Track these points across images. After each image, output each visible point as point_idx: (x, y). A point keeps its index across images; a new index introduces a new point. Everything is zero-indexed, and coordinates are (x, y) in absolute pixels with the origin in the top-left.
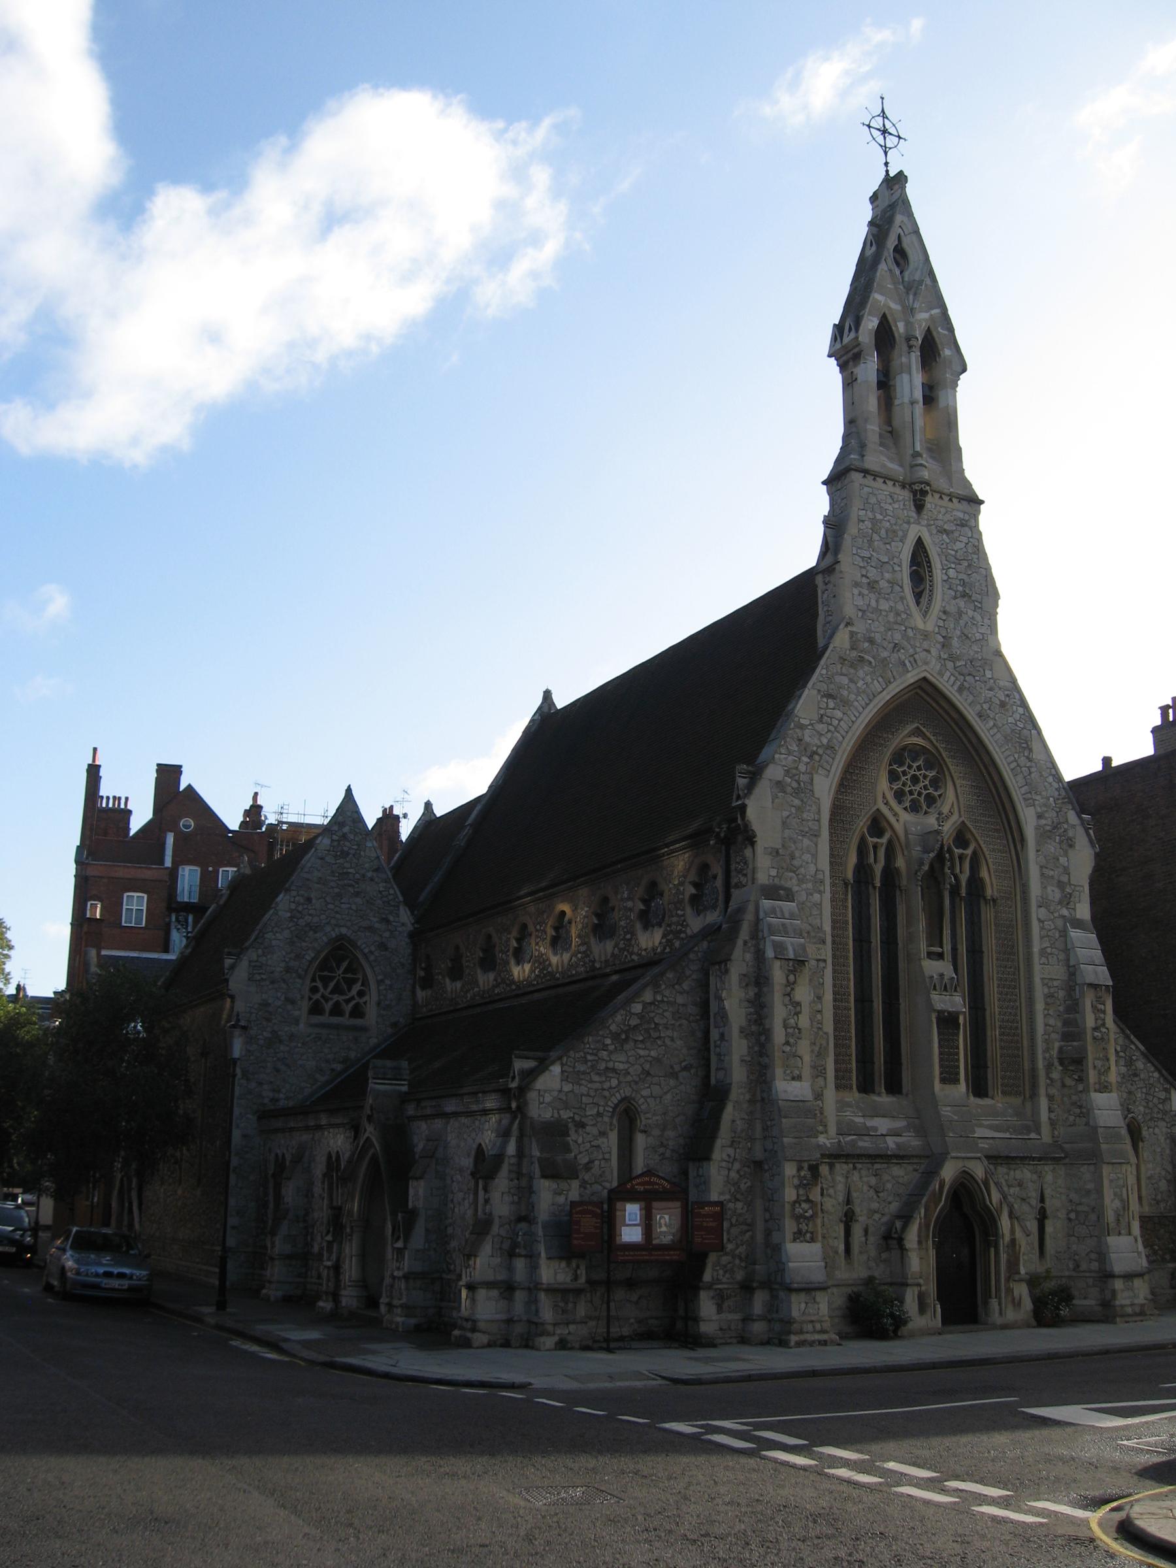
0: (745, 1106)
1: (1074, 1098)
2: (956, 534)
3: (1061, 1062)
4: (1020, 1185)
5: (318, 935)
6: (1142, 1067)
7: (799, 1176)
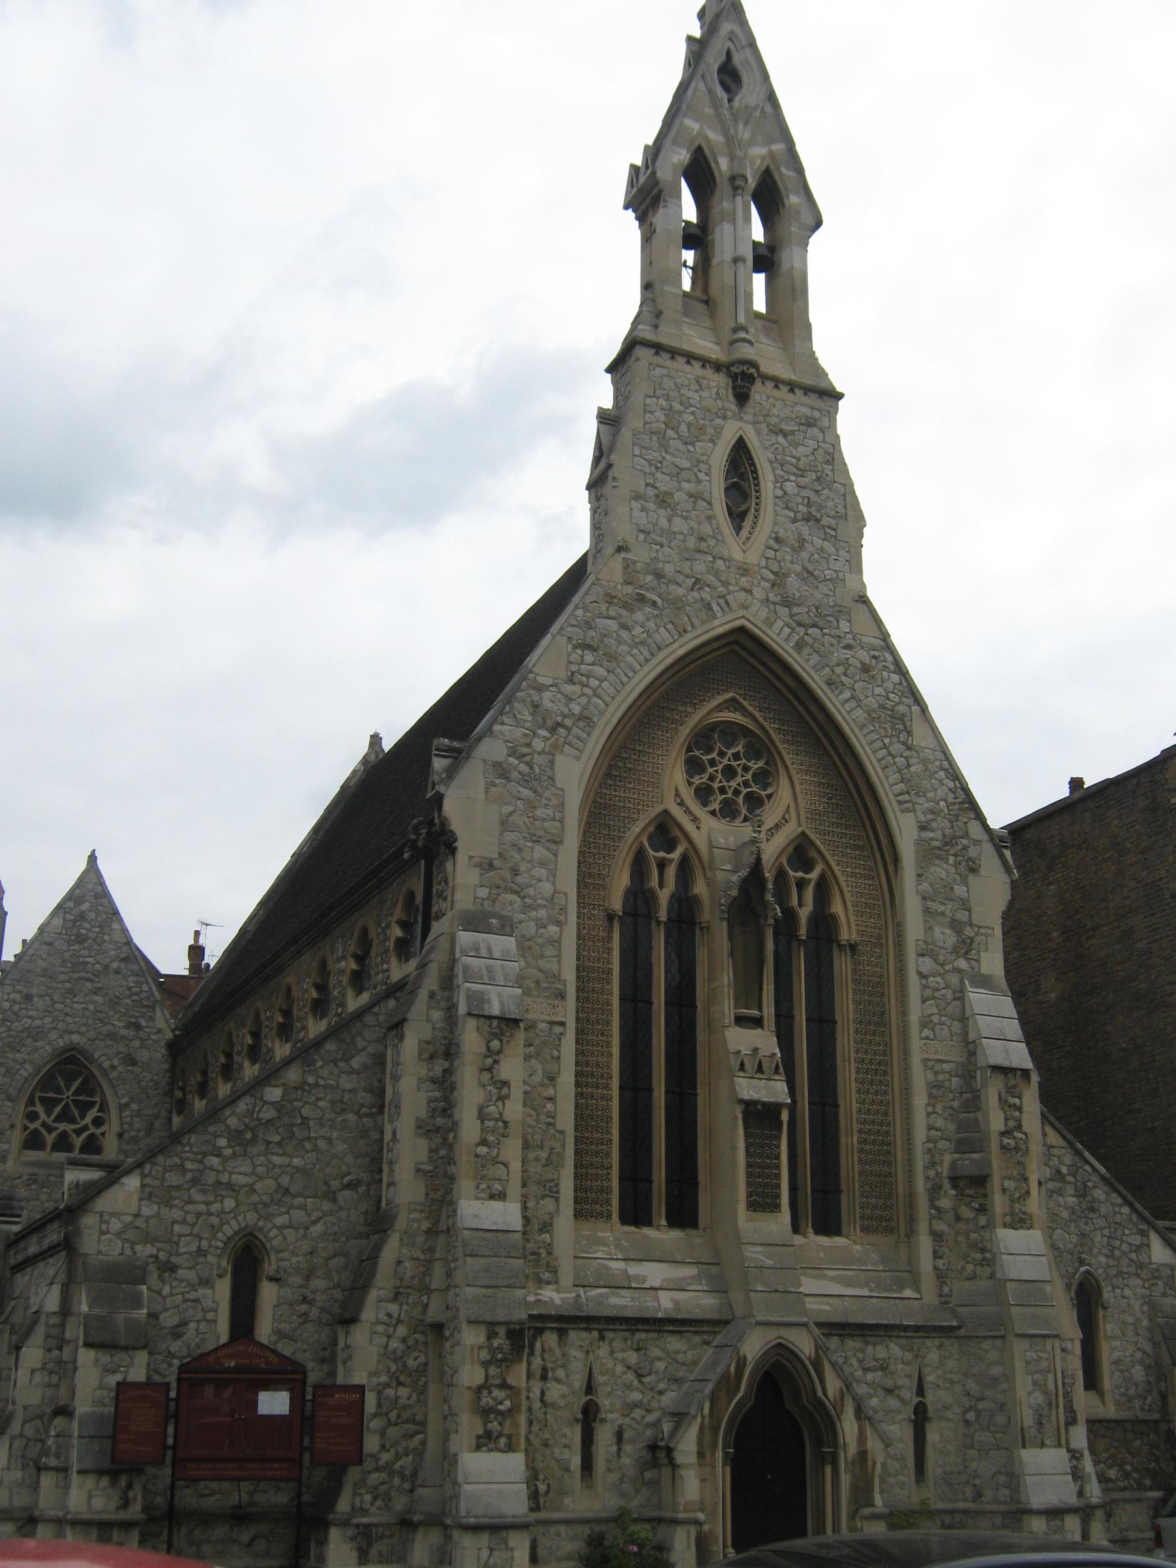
0: (420, 1239)
1: (974, 1236)
2: (799, 436)
3: (954, 1180)
4: (883, 1368)
5: (39, 1044)
6: (1103, 1197)
7: (490, 1347)
